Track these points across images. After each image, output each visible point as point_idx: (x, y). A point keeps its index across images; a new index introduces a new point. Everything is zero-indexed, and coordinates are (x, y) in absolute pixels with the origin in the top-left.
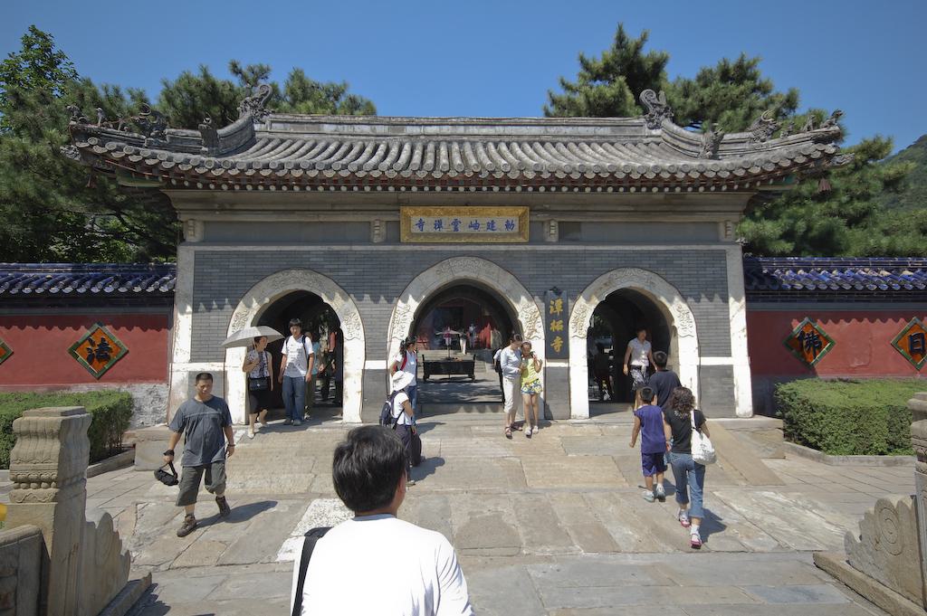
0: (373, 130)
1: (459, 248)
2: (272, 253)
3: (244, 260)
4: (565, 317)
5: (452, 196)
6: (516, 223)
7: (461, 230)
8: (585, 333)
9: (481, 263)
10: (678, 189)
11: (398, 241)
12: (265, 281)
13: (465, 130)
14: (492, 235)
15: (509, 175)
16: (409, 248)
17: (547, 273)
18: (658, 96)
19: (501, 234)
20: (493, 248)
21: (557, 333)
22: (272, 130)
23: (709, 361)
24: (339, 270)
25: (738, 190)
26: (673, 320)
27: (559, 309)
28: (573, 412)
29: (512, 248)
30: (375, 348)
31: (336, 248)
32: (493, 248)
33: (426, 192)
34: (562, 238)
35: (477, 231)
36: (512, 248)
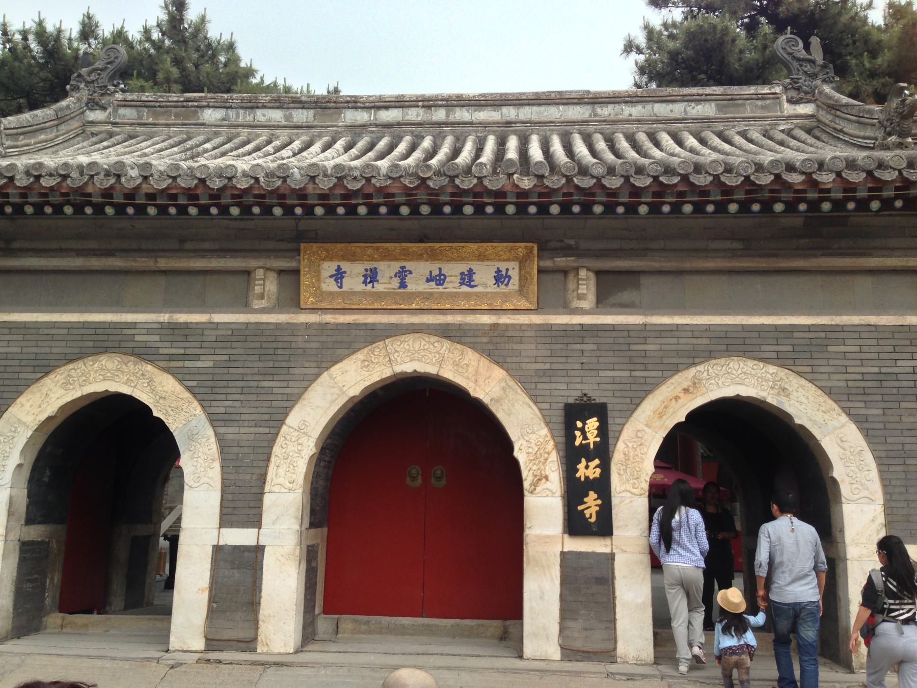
0: (288, 118)
1: (407, 319)
2: (70, 326)
3: (20, 337)
4: (603, 452)
5: (241, 224)
6: (515, 274)
7: (411, 287)
9: (445, 346)
12: (52, 376)
13: (448, 116)
14: (467, 296)
15: (486, 182)
16: (313, 318)
17: (569, 366)
18: (807, 47)
20: (470, 319)
22: (117, 120)
24: (184, 357)
26: (829, 465)
27: (593, 438)
28: (621, 649)
29: (505, 319)
32: (470, 319)
33: (362, 218)
34: (603, 301)
35: (441, 289)
36: (505, 319)
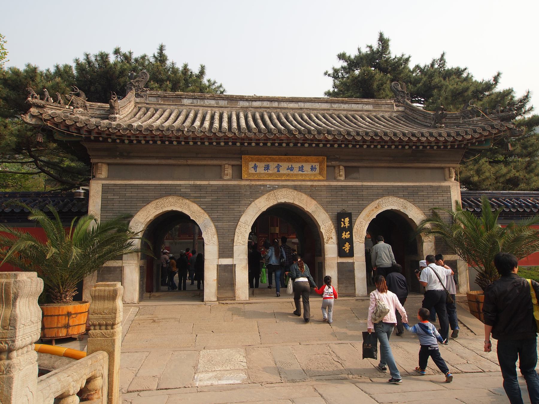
0: (217, 103)
1: (281, 183)
8: (364, 240)
10: (421, 147)
11: (240, 178)
12: (150, 204)
13: (278, 105)
14: (302, 175)
17: (338, 200)
19: (308, 174)
20: (303, 183)
21: (346, 240)
23: (182, 289)
24: (200, 197)
25: (457, 148)
27: (347, 224)
29: (315, 183)
30: (226, 250)
31: (198, 183)
32: (303, 183)
34: (347, 177)
